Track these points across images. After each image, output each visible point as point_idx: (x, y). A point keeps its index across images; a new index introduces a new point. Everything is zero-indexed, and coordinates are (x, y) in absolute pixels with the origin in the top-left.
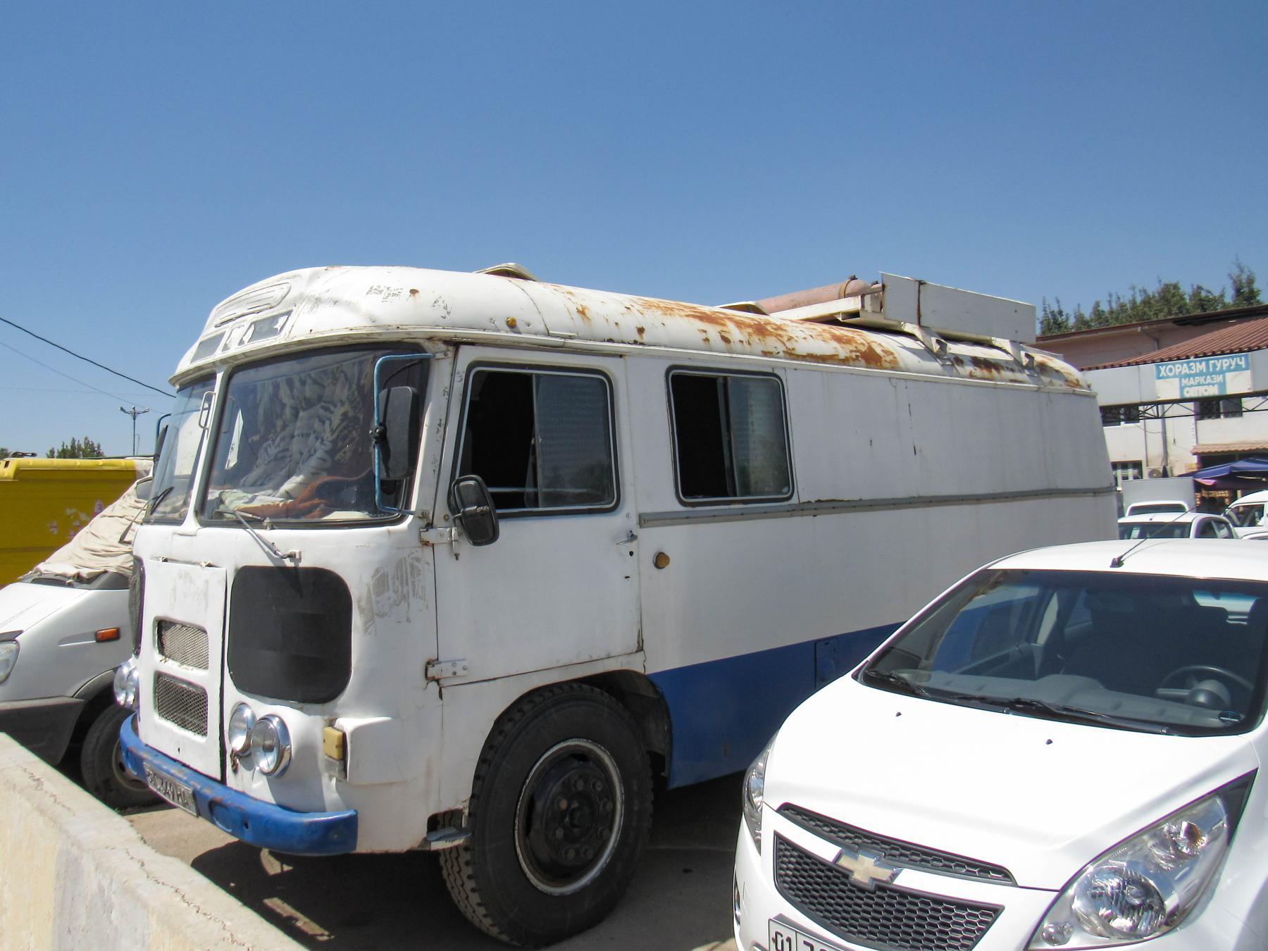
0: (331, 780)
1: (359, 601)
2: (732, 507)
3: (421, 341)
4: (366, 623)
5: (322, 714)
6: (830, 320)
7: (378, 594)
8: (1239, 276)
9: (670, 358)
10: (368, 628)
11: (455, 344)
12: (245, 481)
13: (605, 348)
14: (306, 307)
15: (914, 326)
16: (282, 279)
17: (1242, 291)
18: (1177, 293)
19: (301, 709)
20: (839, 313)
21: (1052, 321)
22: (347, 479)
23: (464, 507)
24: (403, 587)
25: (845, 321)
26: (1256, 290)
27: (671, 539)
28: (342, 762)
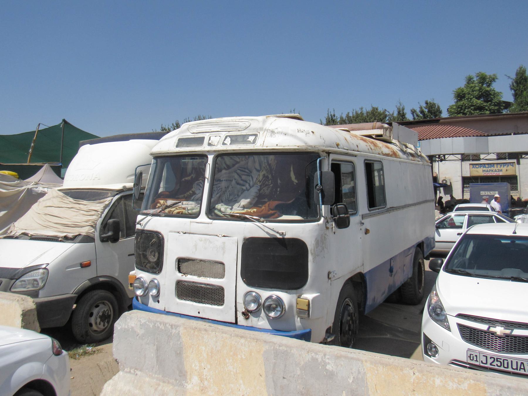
1: (311, 251)
2: (380, 210)
3: (320, 152)
4: (313, 259)
5: (296, 294)
6: (370, 136)
7: (317, 247)
9: (364, 156)
11: (328, 153)
12: (194, 198)
14: (267, 134)
15: (396, 141)
16: (242, 119)
19: (287, 292)
21: (331, 119)
22: (286, 203)
23: (339, 214)
25: (376, 138)
27: (368, 223)
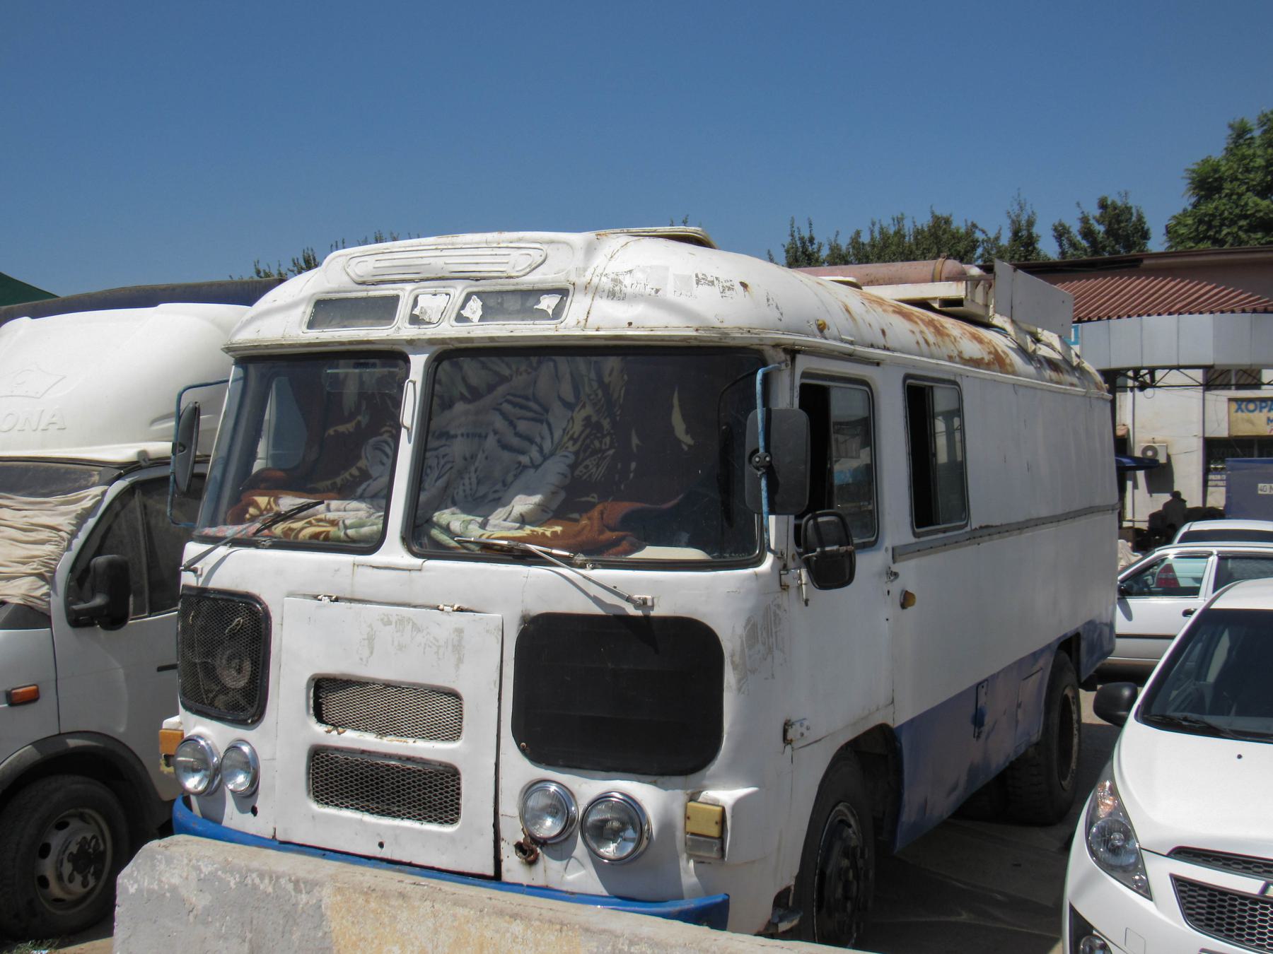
0: (688, 862)
1: (732, 656)
6: (924, 304)
8: (1018, 216)
10: (741, 687)
11: (792, 352)
12: (365, 490)
13: (870, 356)
15: (1006, 319)
17: (1020, 234)
18: (948, 229)
19: (654, 783)
20: (935, 299)
23: (822, 545)
24: (768, 638)
26: (1034, 235)
27: (911, 573)
28: (720, 840)
